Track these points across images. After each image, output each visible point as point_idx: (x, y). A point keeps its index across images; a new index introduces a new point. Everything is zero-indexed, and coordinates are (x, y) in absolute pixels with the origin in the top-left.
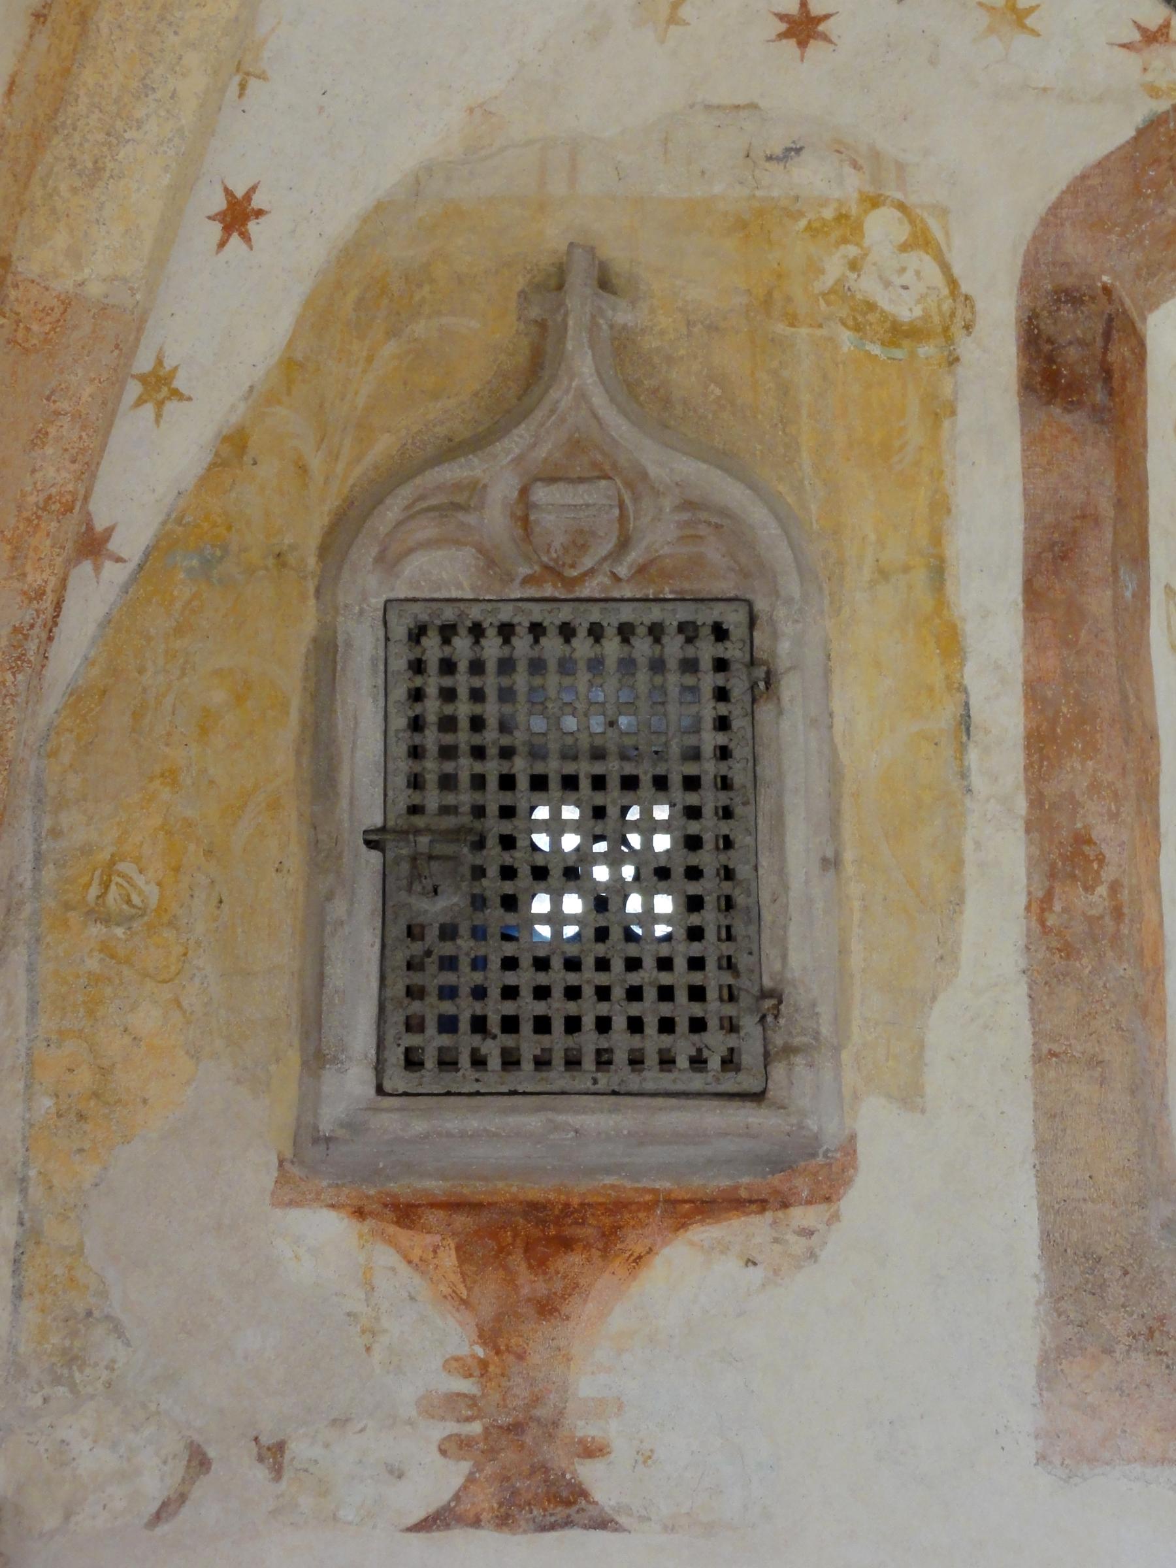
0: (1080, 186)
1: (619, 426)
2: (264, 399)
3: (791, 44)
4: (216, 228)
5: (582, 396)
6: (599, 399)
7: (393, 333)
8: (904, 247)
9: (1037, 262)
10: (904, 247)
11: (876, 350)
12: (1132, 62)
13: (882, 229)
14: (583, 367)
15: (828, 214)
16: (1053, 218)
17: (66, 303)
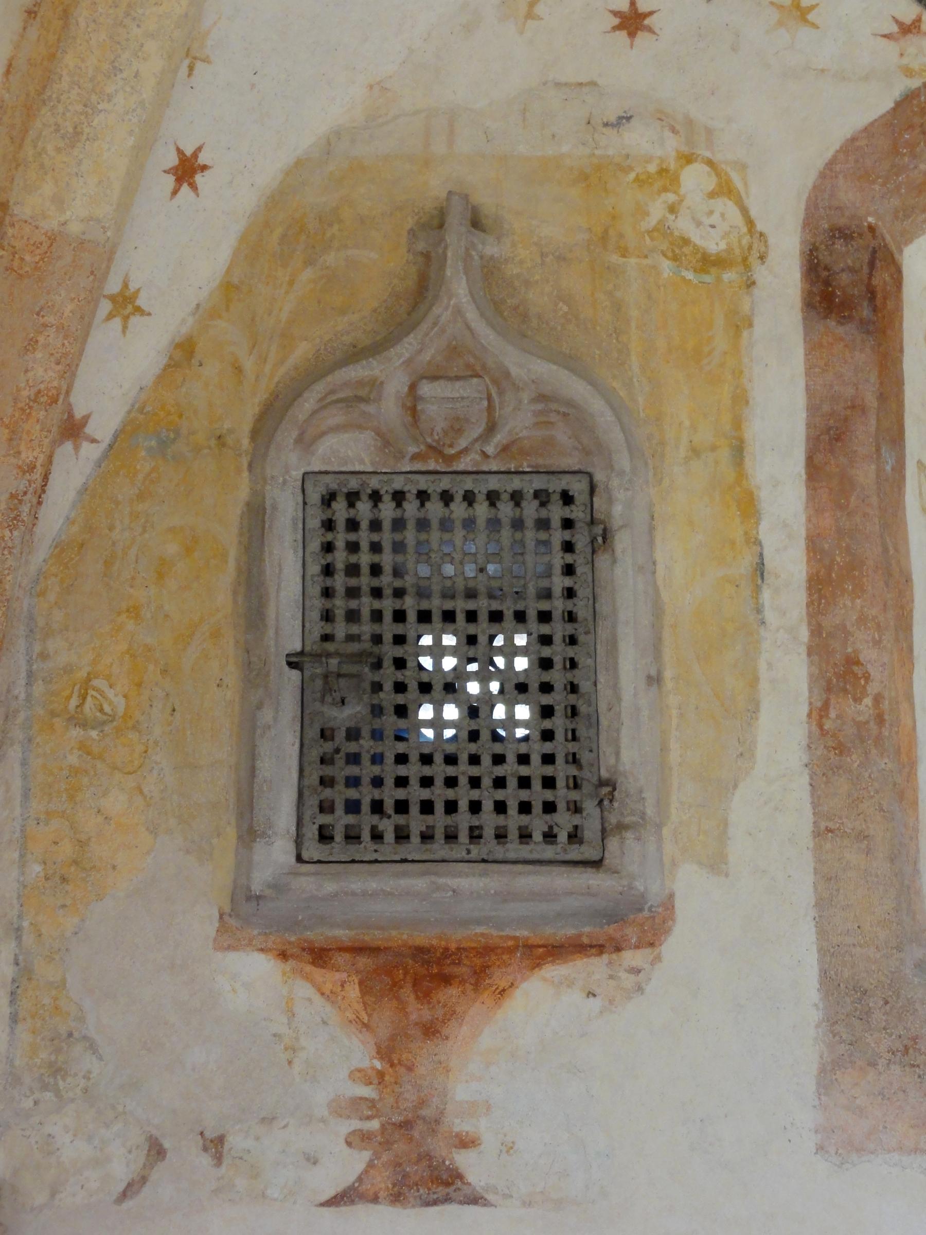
0: (850, 146)
1: (487, 335)
2: (208, 314)
3: (622, 35)
4: (170, 180)
5: (458, 312)
6: (472, 315)
7: (309, 262)
8: (712, 195)
9: (816, 207)
10: (712, 195)
11: (690, 275)
12: (891, 49)
13: (695, 180)
14: (459, 289)
15: (652, 168)
16: (829, 171)
17: (52, 239)
